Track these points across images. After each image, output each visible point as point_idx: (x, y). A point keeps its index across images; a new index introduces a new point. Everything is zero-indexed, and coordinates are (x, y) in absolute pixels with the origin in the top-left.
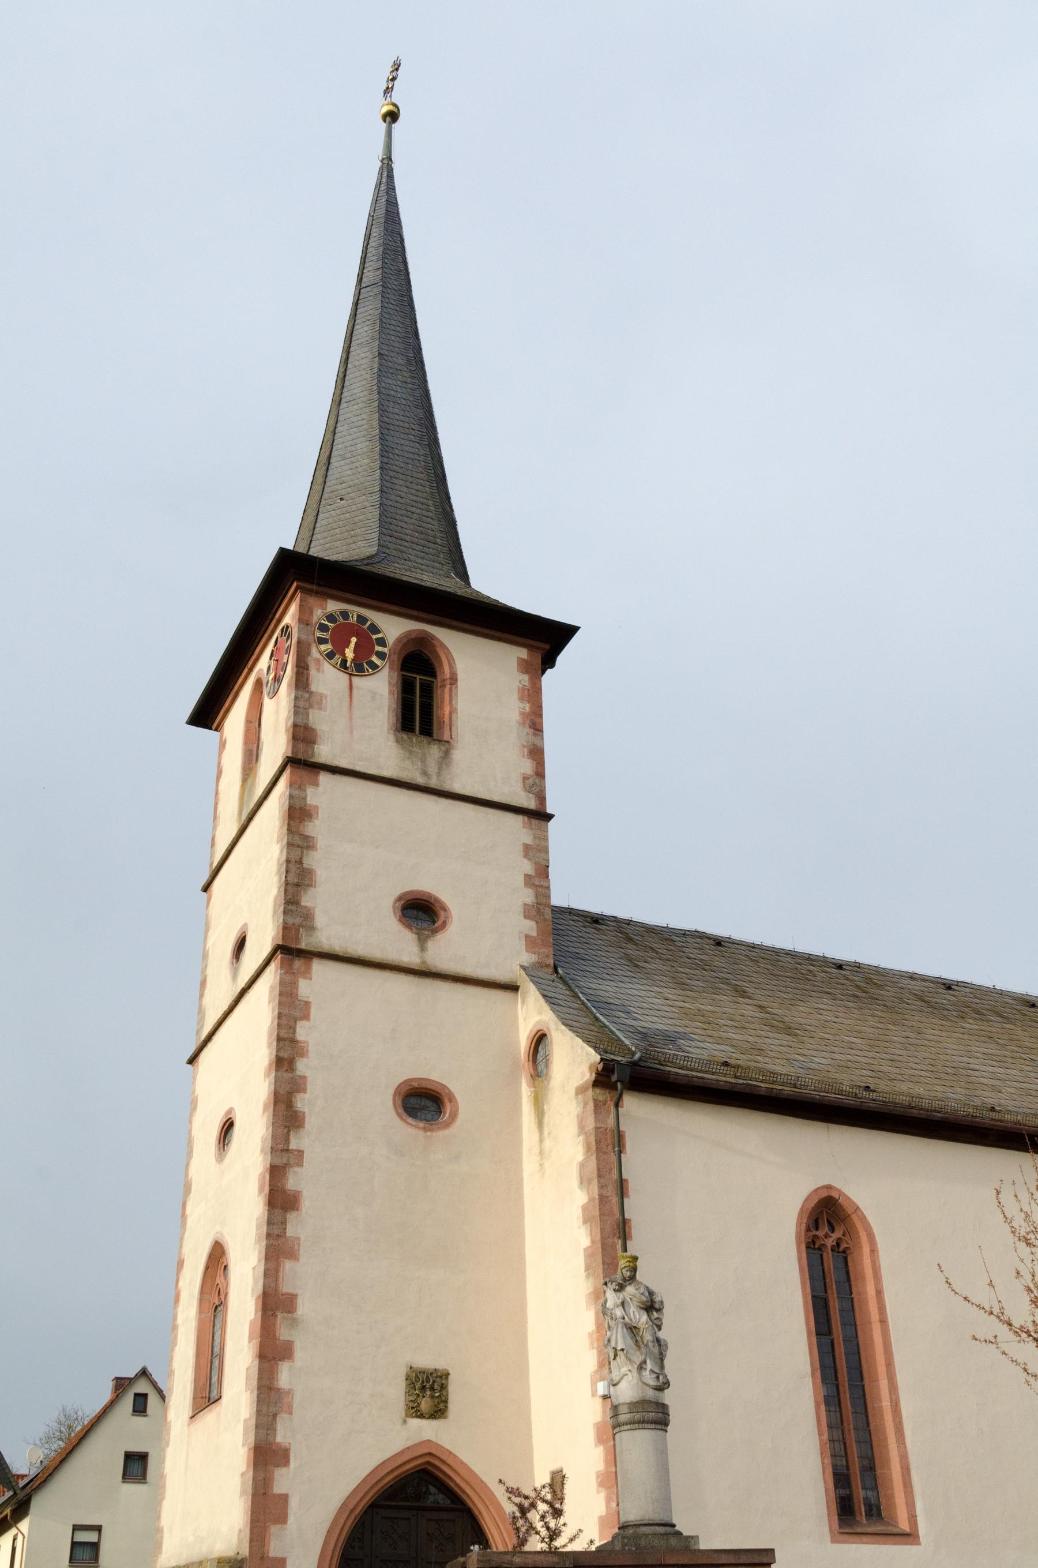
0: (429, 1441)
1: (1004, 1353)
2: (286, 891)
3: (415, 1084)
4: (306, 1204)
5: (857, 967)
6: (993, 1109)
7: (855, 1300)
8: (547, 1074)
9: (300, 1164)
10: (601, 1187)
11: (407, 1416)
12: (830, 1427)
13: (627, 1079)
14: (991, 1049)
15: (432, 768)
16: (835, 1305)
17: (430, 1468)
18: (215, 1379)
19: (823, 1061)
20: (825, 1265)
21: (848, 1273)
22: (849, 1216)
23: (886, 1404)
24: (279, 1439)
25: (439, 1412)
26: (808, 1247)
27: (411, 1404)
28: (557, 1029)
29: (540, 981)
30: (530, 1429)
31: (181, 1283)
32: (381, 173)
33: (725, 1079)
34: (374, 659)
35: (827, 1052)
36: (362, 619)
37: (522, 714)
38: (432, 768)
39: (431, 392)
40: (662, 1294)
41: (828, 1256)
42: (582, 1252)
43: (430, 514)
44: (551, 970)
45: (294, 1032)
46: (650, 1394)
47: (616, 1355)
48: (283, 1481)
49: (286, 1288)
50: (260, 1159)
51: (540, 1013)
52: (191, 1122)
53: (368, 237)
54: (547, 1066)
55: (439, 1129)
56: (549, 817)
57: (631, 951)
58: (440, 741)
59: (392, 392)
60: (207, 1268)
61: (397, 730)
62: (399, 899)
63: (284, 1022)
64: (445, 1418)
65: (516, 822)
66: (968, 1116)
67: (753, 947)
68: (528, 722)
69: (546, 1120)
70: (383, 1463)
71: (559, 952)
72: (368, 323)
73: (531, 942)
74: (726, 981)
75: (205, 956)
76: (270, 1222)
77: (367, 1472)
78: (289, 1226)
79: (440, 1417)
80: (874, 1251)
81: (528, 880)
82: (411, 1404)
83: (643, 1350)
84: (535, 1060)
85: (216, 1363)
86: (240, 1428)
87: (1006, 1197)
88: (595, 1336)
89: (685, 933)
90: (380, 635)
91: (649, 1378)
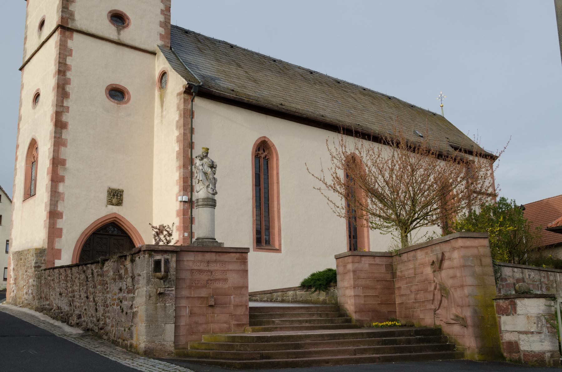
2: (63, 3)
3: (114, 86)
4: (70, 127)
5: (281, 62)
9: (68, 112)
10: (184, 130)
13: (197, 92)
14: (324, 96)
16: (262, 177)
18: (33, 188)
23: (276, 209)
24: (59, 210)
31: (18, 153)
33: (232, 95)
35: (269, 91)
41: (262, 161)
44: (169, 48)
45: (66, 61)
46: (210, 196)
48: (60, 224)
49: (62, 157)
50: (52, 109)
51: (164, 64)
52: (21, 93)
54: (166, 85)
57: (200, 45)
60: (29, 148)
62: (110, 12)
63: (62, 56)
67: (244, 50)
69: (164, 105)
71: (172, 42)
73: (162, 37)
74: (234, 61)
75: (26, 27)
76: (55, 132)
78: (63, 134)
80: (277, 160)
81: (162, 12)
84: (161, 82)
85: (33, 182)
86: (44, 205)
89: (220, 42)
91: (210, 190)
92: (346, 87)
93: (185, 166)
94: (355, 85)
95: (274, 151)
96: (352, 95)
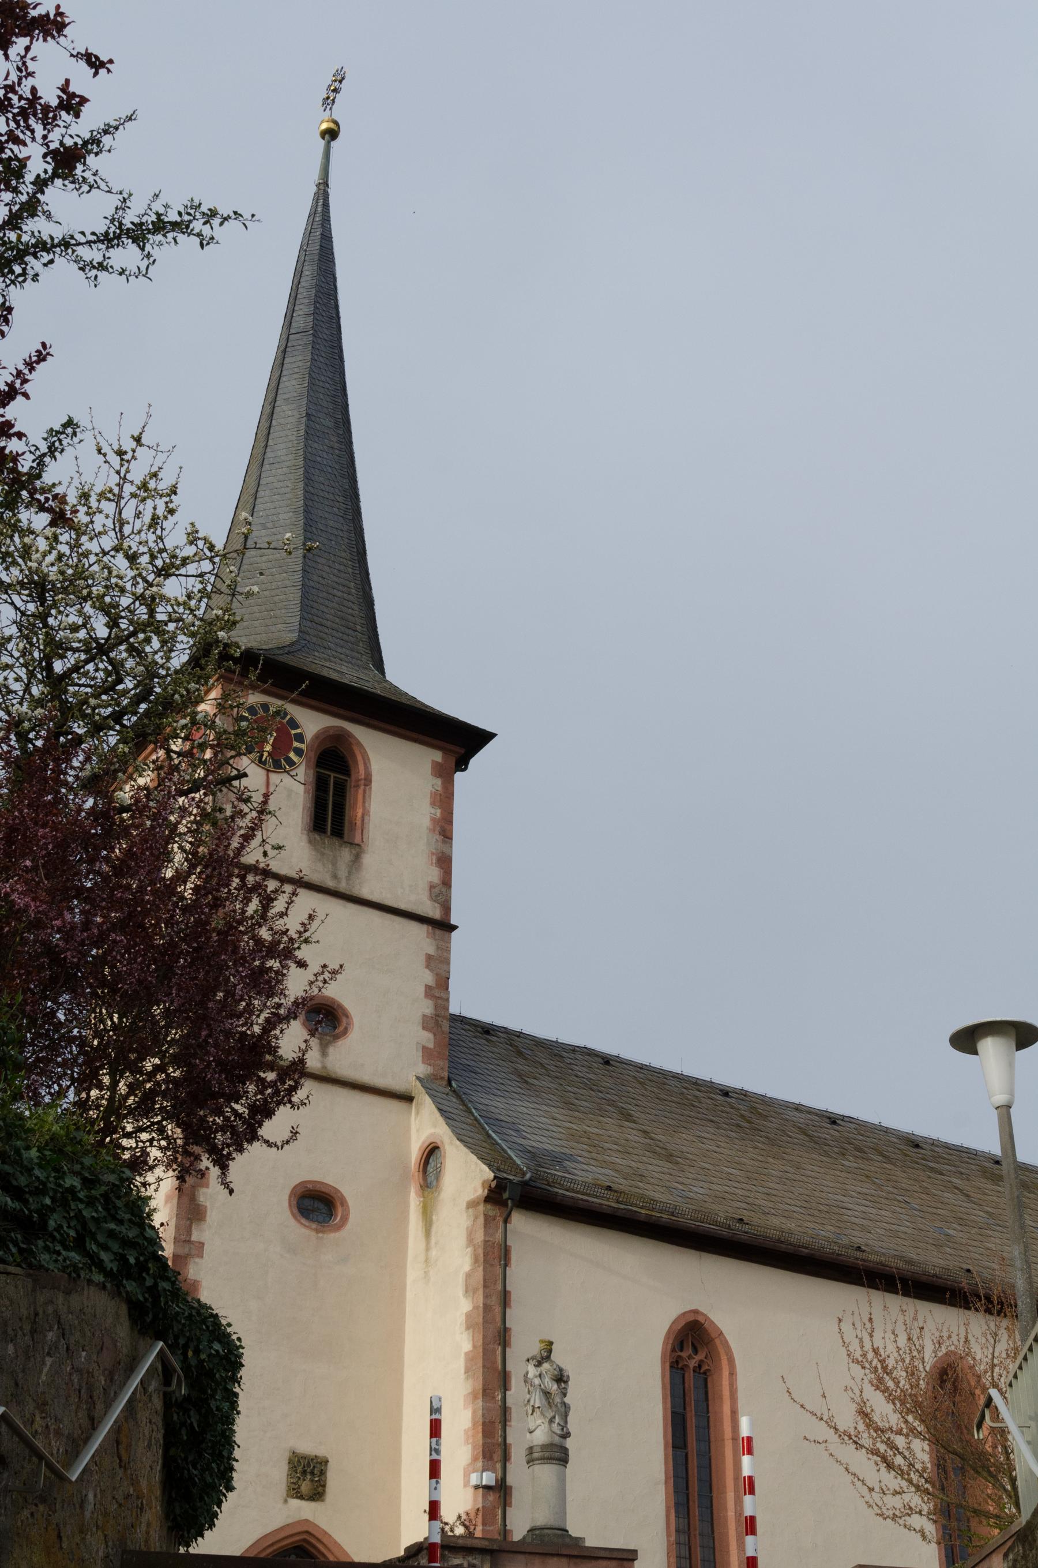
0: (307, 1520)
1: (831, 1455)
3: (310, 1186)
5: (744, 1094)
6: (859, 1248)
7: (711, 1419)
8: (437, 1186)
10: (486, 1296)
11: (288, 1496)
12: (678, 1531)
15: (343, 872)
17: (304, 1544)
19: (701, 1191)
20: (686, 1385)
21: (706, 1393)
22: (713, 1340)
25: (317, 1495)
26: (671, 1367)
27: (293, 1486)
28: (451, 1143)
29: (435, 1093)
30: (399, 1517)
32: (316, 199)
33: (608, 1203)
34: (292, 755)
35: (706, 1181)
36: (280, 713)
37: (433, 820)
38: (343, 872)
39: (356, 455)
40: (570, 1370)
41: (690, 1376)
42: (463, 1355)
43: (350, 597)
44: (445, 1083)
47: (533, 1411)
51: (435, 1126)
53: (299, 273)
55: (331, 1231)
56: (454, 928)
57: (522, 1066)
58: (351, 844)
59: (319, 459)
61: (309, 831)
64: (323, 1501)
65: (419, 931)
66: (833, 1253)
67: (641, 1067)
68: (438, 829)
70: (265, 1536)
72: (296, 376)
73: (427, 1054)
74: (612, 1103)
77: (250, 1543)
79: (318, 1500)
80: (732, 1374)
82: (293, 1486)
83: (554, 1409)
87: (846, 1327)
88: (470, 1433)
89: (574, 1049)
90: (299, 731)
92: (937, 1158)
93: (486, 1392)
94: (968, 1151)
95: (722, 1351)
96: (957, 1181)
